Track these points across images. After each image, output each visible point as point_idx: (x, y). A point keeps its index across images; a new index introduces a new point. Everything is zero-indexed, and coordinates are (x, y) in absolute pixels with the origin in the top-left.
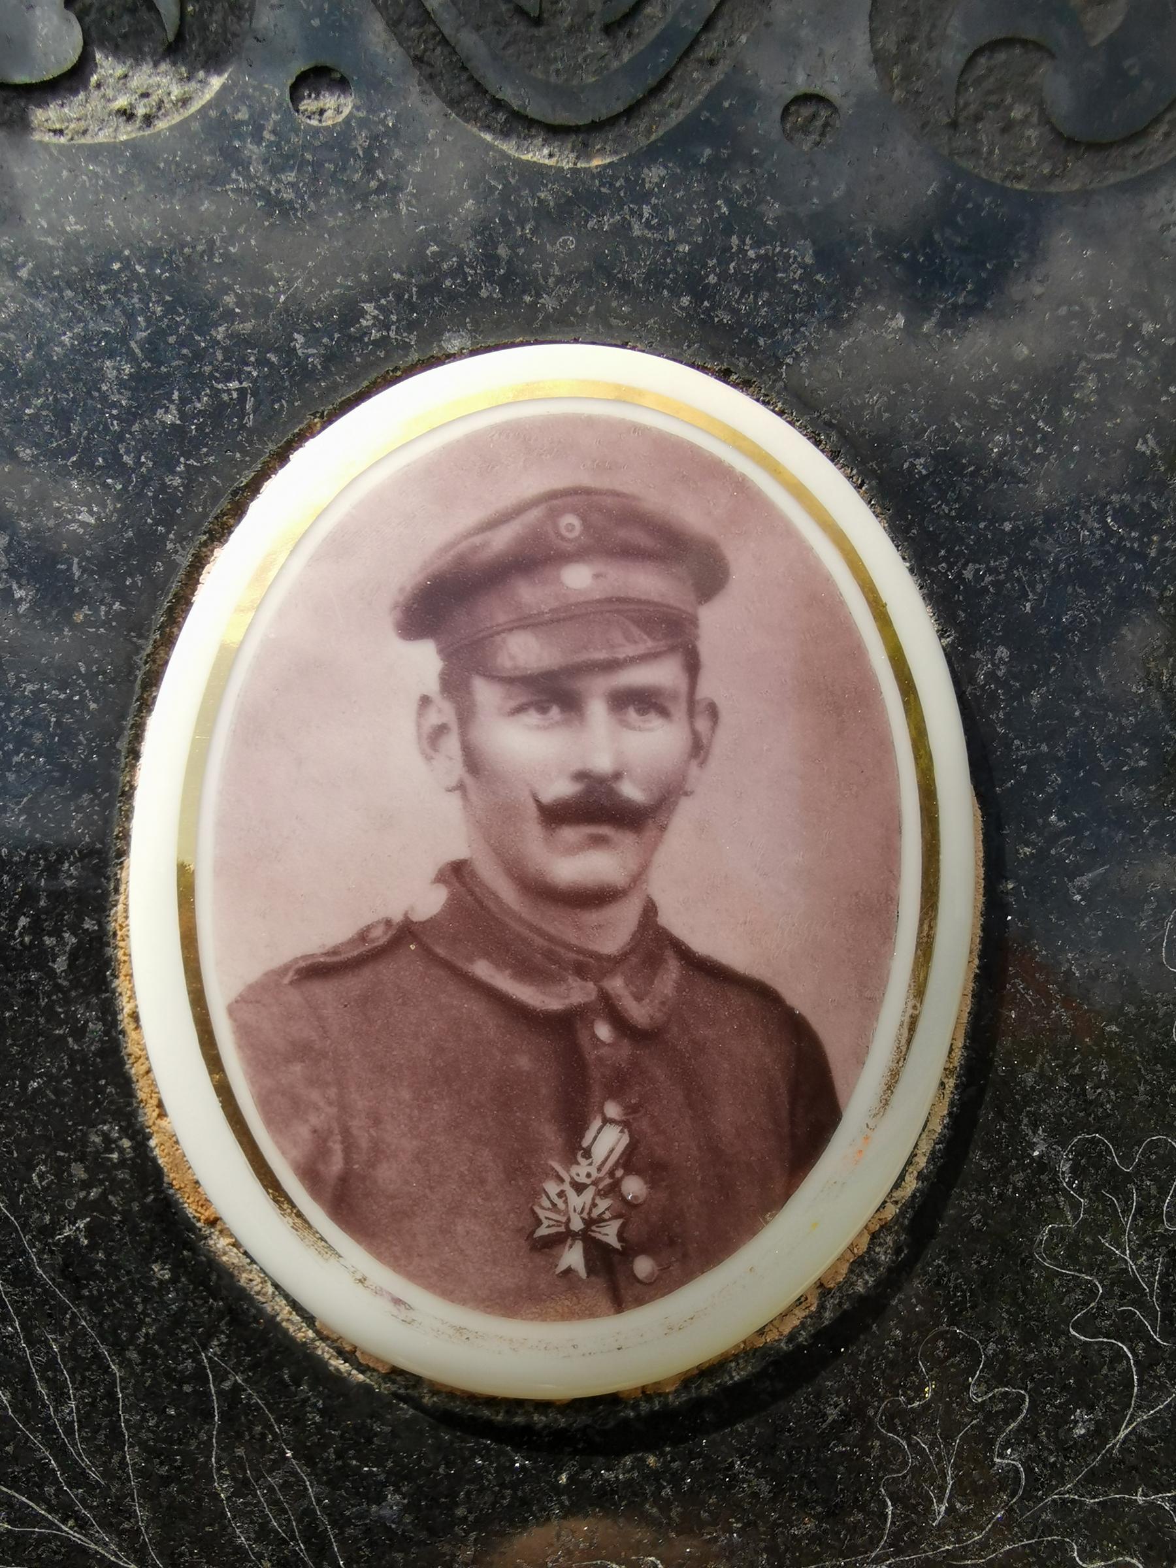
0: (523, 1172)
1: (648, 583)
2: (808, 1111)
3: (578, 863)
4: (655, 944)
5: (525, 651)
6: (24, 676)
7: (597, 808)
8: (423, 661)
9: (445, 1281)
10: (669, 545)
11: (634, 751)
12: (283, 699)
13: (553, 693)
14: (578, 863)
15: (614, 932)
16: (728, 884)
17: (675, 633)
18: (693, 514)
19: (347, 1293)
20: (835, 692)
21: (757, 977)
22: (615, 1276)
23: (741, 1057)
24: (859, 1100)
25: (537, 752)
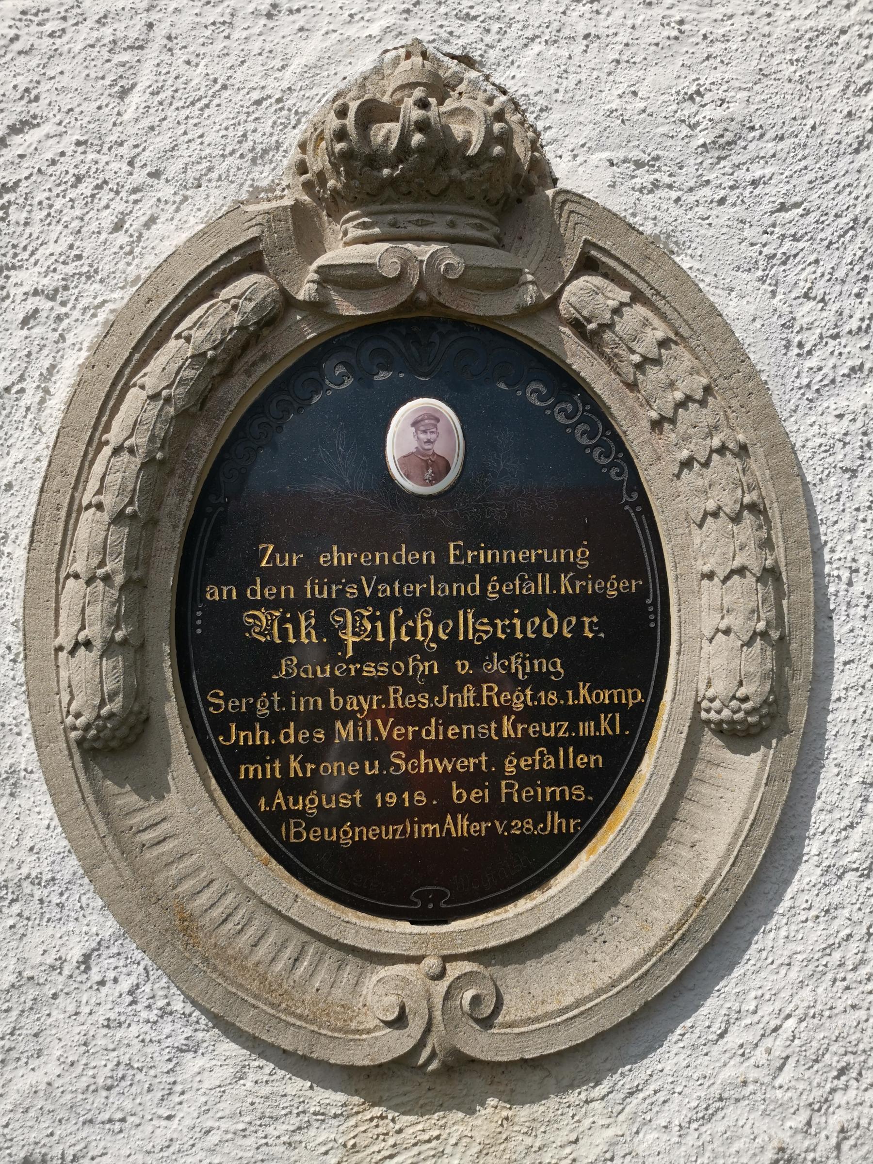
0: (423, 474)
1: (433, 422)
2: (448, 468)
3: (427, 447)
4: (434, 454)
5: (422, 428)
6: (417, 433)
7: (429, 442)
8: (413, 429)
9: (416, 483)
10: (438, 420)
11: (432, 437)
12: (400, 435)
13: (425, 432)
14: (427, 447)
15: (431, 453)
16: (440, 448)
17: (435, 426)
18: (437, 415)
19: (408, 485)
20: (450, 431)
21: (379, 919)
22: (431, 483)
23: (442, 463)
24: (452, 467)
25: (423, 436)
